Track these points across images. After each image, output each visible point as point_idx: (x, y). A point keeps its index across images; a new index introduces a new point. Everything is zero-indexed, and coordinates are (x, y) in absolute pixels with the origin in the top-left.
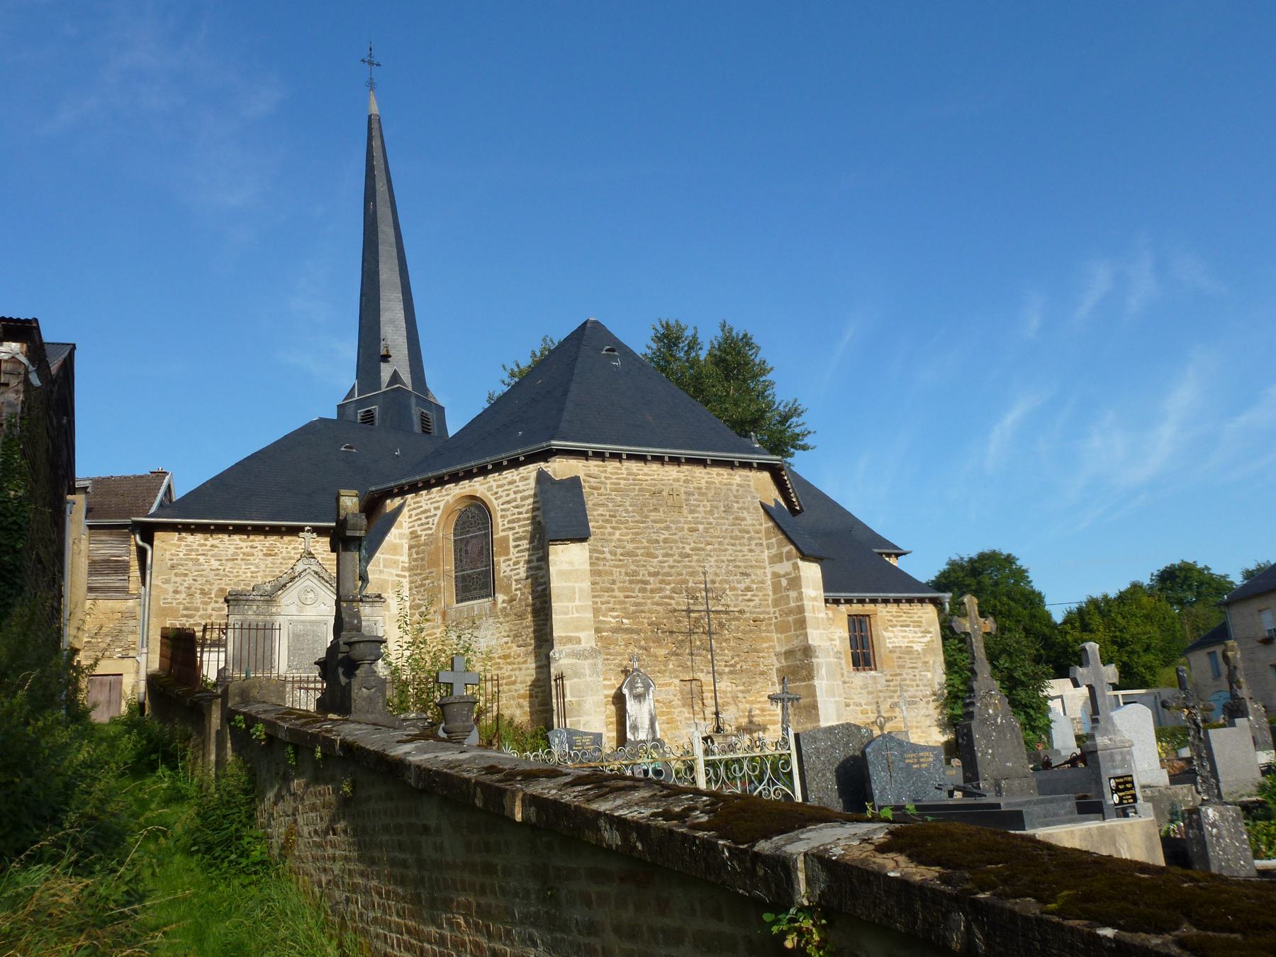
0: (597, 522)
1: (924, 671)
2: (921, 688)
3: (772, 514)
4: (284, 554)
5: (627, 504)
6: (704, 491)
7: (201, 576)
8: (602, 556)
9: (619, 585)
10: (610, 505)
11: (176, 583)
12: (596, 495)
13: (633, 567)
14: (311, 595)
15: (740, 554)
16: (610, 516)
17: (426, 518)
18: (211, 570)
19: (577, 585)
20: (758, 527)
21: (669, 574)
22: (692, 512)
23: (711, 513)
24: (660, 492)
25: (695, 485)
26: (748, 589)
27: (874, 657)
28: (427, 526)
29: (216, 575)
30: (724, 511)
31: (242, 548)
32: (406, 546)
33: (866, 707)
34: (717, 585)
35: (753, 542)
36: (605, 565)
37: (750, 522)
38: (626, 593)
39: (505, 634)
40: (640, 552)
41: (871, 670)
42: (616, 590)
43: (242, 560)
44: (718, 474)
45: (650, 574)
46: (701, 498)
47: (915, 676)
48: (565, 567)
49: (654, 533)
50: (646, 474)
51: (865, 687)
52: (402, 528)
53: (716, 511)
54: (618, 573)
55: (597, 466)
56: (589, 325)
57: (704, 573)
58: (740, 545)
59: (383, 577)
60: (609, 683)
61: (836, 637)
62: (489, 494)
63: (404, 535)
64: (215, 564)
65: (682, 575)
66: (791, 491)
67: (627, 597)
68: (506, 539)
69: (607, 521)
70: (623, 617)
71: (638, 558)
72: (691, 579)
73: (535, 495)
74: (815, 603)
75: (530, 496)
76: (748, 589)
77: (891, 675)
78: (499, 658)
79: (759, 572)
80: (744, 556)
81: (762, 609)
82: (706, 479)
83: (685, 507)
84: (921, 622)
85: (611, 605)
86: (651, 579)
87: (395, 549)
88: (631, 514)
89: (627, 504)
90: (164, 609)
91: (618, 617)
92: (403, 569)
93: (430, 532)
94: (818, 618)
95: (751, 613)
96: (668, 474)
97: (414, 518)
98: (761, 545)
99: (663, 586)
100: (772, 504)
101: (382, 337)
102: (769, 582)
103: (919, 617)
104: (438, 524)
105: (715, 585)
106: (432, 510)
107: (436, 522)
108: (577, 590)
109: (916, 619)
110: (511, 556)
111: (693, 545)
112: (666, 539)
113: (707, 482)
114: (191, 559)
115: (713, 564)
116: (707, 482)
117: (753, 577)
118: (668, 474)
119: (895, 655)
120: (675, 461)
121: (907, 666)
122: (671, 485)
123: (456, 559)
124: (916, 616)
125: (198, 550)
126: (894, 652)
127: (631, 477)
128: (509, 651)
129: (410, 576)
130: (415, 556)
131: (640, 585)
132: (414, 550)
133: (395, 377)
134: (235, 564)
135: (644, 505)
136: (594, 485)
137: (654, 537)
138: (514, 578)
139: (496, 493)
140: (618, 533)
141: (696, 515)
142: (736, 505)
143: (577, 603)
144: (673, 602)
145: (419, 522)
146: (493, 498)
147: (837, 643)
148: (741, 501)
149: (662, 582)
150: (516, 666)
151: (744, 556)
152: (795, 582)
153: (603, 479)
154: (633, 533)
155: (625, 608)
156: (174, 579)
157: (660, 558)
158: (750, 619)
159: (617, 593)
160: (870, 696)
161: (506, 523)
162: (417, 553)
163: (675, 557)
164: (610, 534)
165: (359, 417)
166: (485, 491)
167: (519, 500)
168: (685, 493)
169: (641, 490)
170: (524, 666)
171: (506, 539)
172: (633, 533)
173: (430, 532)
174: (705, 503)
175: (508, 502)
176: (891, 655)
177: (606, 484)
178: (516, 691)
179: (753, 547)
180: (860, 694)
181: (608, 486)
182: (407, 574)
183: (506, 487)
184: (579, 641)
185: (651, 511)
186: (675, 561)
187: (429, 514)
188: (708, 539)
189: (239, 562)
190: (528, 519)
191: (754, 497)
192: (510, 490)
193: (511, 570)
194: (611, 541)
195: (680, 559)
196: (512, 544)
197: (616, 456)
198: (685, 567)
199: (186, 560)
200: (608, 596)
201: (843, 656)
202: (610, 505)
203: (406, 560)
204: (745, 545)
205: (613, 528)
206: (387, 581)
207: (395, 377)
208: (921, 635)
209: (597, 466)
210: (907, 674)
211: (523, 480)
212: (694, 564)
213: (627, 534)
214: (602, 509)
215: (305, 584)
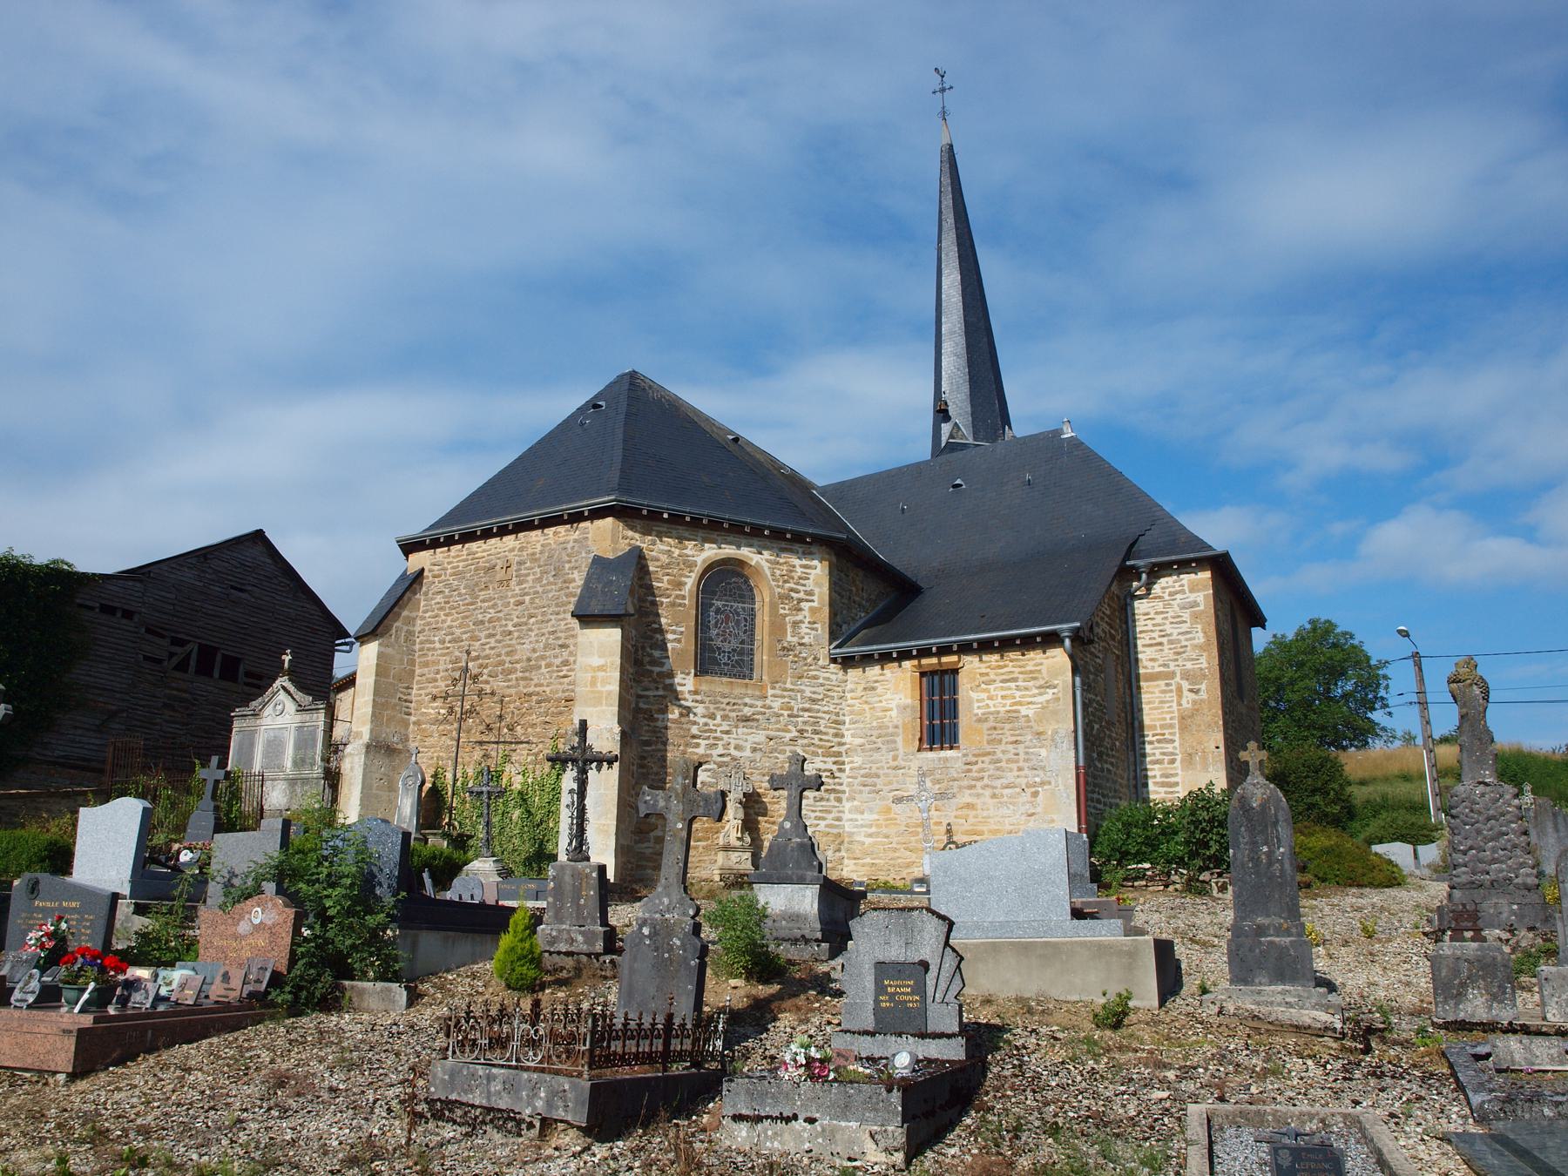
0: (433, 611)
2: (1026, 772)
8: (432, 646)
9: (442, 674)
15: (563, 623)
21: (487, 657)
25: (530, 551)
34: (533, 663)
40: (464, 637)
44: (555, 533)
47: (1017, 754)
50: (484, 551)
55: (442, 552)
61: (893, 705)
69: (441, 609)
72: (508, 659)
77: (974, 755)
94: (601, 692)
103: (1036, 665)
111: (516, 620)
119: (986, 726)
120: (503, 531)
121: (1004, 740)
126: (986, 720)
127: (470, 557)
137: (480, 617)
140: (449, 619)
142: (567, 566)
147: (894, 713)
154: (463, 618)
157: (483, 641)
163: (497, 637)
169: (476, 569)
176: (979, 726)
185: (481, 590)
198: (504, 646)
201: (900, 731)
202: (447, 590)
208: (1037, 691)
209: (442, 552)
210: (1004, 752)
212: (514, 642)
213: (458, 619)
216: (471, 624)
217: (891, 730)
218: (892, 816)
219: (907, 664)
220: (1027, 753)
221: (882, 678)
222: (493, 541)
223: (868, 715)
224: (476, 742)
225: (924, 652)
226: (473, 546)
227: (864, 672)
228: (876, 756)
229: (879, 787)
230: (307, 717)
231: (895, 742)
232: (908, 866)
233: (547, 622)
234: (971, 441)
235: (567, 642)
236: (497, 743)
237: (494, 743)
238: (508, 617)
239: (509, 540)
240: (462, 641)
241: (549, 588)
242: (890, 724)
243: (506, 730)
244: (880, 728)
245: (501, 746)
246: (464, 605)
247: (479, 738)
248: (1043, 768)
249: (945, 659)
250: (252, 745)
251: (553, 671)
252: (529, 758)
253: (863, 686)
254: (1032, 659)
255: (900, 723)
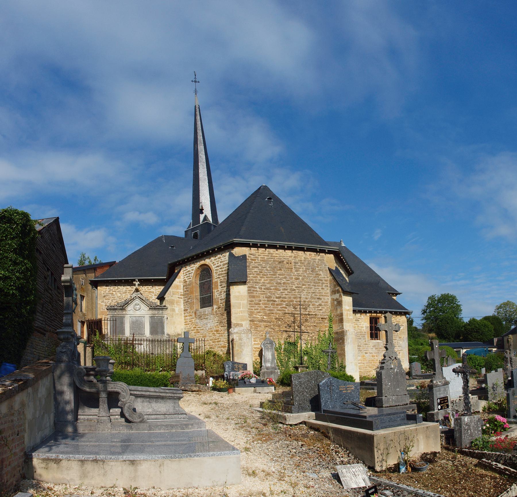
0: (254, 275)
1: (399, 341)
3: (332, 272)
4: (144, 290)
5: (268, 267)
6: (303, 262)
7: (114, 299)
8: (256, 289)
9: (262, 302)
10: (260, 267)
11: (106, 302)
12: (254, 262)
13: (269, 294)
14: (138, 306)
15: (318, 290)
16: (260, 272)
17: (189, 274)
18: (118, 297)
19: (242, 302)
20: (326, 279)
21: (285, 298)
22: (296, 271)
23: (306, 271)
24: (283, 262)
25: (299, 259)
26: (320, 305)
27: (379, 334)
28: (189, 277)
29: (120, 299)
30: (311, 271)
31: (128, 288)
32: (182, 286)
33: (374, 354)
34: (306, 303)
35: (324, 285)
36: (256, 293)
37: (323, 276)
38: (266, 306)
39: (217, 322)
40: (272, 288)
41: (378, 340)
42: (261, 304)
43: (129, 293)
44: (310, 255)
45: (277, 298)
46: (301, 265)
48: (237, 294)
49: (279, 280)
50: (277, 254)
51: (374, 346)
52: (180, 278)
53: (308, 271)
54: (262, 297)
55: (254, 250)
56: (262, 188)
57: (300, 298)
58: (318, 286)
59: (172, 298)
60: (257, 343)
61: (364, 326)
62: (211, 263)
63: (181, 281)
64: (119, 295)
65: (290, 298)
66: (345, 262)
67: (266, 307)
68: (217, 282)
69: (258, 274)
70: (264, 316)
71: (271, 291)
72: (295, 300)
73: (228, 263)
74: (348, 312)
75: (226, 263)
76: (320, 305)
78: (215, 331)
79: (326, 298)
80: (319, 291)
81: (326, 314)
82: (304, 257)
83: (294, 269)
84: (400, 321)
85: (259, 311)
86: (277, 300)
87: (177, 287)
88: (269, 271)
89: (268, 267)
90: (102, 312)
91: (261, 315)
92: (181, 295)
93: (190, 280)
94: (349, 318)
95: (321, 315)
96: (287, 254)
97: (185, 274)
98: (327, 286)
99: (282, 303)
100: (334, 269)
101: (200, 202)
102: (329, 302)
103: (399, 320)
104: (193, 276)
105: (306, 303)
106: (191, 271)
107: (192, 276)
108: (241, 304)
109: (398, 320)
110: (219, 289)
111: (296, 285)
112: (285, 282)
113: (304, 258)
114: (110, 293)
115: (305, 294)
116: (304, 258)
117: (323, 300)
118: (287, 254)
120: (290, 248)
122: (288, 259)
123: (200, 291)
124: (398, 319)
125: (113, 290)
127: (270, 255)
128: (218, 328)
129: (184, 298)
130: (185, 290)
131: (272, 302)
132: (185, 287)
133: (206, 218)
134: (126, 294)
135: (275, 267)
136: (253, 258)
137: (279, 281)
138: (220, 298)
139: (214, 263)
140: (263, 279)
141: (299, 272)
142: (317, 269)
143: (241, 309)
144: (286, 309)
145: (187, 276)
146: (212, 265)
147: (364, 328)
148: (319, 267)
149: (282, 301)
150: (220, 335)
151: (319, 291)
152: (340, 303)
153: (257, 256)
154: (270, 280)
155: (265, 312)
156: (105, 301)
157: (282, 291)
158: (320, 318)
159: (261, 305)
160: (376, 350)
161: (217, 275)
162: (186, 289)
163: (288, 290)
164: (260, 280)
165: (192, 235)
166: (210, 262)
167: (222, 265)
168: (294, 262)
169: (274, 261)
170: (223, 335)
171: (217, 282)
172: (270, 280)
173: (190, 280)
174: (303, 267)
175: (218, 266)
177: (258, 258)
178: (221, 344)
179: (324, 287)
180: (372, 349)
181: (259, 259)
182: (182, 297)
183: (217, 260)
184: (242, 325)
186: (288, 292)
187: (190, 272)
188: (304, 283)
189: (127, 293)
190: (225, 273)
191: (325, 265)
192: (219, 261)
193: (219, 295)
194: (260, 283)
195: (290, 291)
196: (219, 284)
197: (263, 246)
199: (109, 294)
200: (258, 307)
201: (366, 334)
202: (260, 267)
203: (182, 291)
204: (320, 286)
205: (261, 277)
206: (174, 300)
207: (206, 218)
209: (254, 250)
211: (224, 257)
212: (297, 294)
213: (267, 280)
214: (256, 269)
215: (136, 302)
216: (275, 283)
217: (364, 333)
218: (365, 358)
219: (368, 315)
220: (397, 342)
221: (360, 318)
222: (281, 251)
223: (357, 328)
224: (283, 331)
225: (376, 312)
226: (272, 251)
227: (355, 315)
228: (360, 340)
229: (361, 349)
230: (156, 312)
231: (365, 337)
232: (370, 372)
233: (311, 288)
234: (212, 223)
235: (321, 297)
236: (294, 332)
237: (292, 332)
238: (292, 283)
239: (289, 252)
240: (271, 289)
241: (310, 275)
242: (363, 331)
243: (296, 327)
244: (361, 332)
245: (296, 333)
246: (270, 275)
247: (285, 329)
248: (401, 346)
249: (378, 315)
250: (122, 323)
251: (315, 307)
252: (309, 338)
253: (355, 319)
254: (398, 318)
255: (366, 331)
